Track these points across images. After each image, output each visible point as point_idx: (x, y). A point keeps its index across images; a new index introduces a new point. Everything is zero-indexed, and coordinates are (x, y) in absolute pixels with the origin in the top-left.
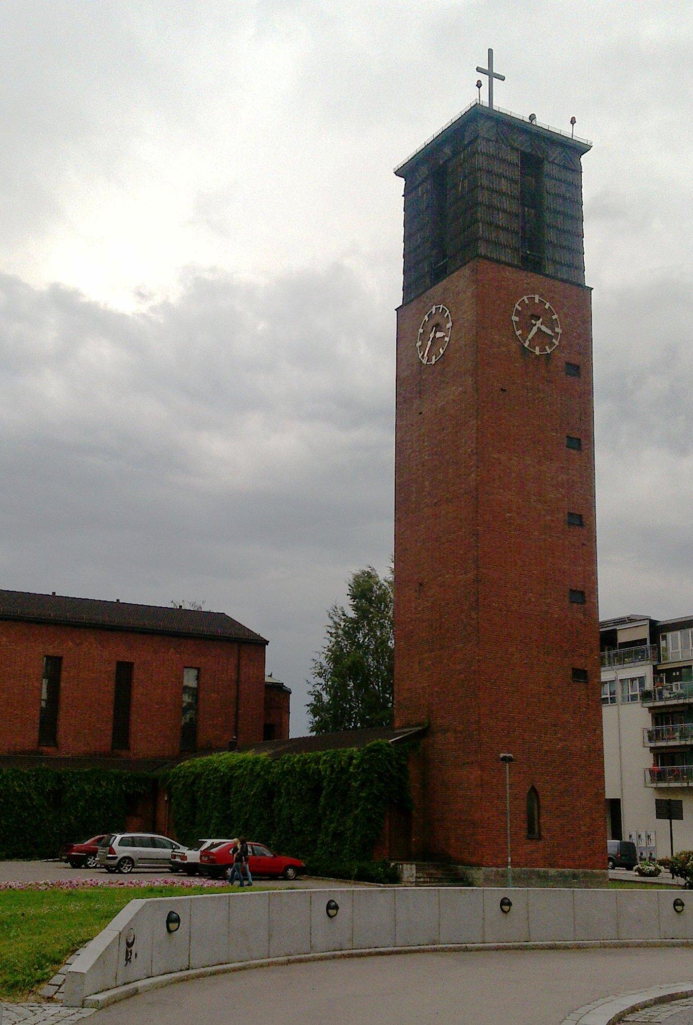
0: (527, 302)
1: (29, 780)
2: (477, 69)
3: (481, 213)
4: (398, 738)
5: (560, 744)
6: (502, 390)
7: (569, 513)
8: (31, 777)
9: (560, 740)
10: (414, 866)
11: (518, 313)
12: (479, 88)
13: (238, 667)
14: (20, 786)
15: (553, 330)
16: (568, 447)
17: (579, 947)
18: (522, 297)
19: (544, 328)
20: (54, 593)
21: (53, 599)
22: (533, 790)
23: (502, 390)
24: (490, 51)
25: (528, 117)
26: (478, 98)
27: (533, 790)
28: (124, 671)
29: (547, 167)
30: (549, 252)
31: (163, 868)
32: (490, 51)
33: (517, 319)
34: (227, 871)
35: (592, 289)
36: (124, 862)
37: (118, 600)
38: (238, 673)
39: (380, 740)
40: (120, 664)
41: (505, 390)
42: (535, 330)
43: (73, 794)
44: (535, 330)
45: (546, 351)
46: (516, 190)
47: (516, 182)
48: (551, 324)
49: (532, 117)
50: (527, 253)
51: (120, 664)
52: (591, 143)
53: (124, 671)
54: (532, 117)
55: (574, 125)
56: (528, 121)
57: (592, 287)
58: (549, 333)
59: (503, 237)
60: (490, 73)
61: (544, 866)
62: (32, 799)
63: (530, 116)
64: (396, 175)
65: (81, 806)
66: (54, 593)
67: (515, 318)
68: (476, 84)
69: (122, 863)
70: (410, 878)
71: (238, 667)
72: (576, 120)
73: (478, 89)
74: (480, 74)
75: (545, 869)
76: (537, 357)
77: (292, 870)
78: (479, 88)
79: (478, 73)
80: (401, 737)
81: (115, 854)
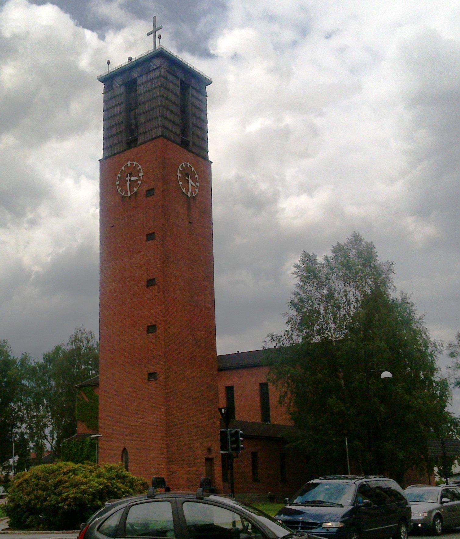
19: (132, 178)
44: (128, 183)
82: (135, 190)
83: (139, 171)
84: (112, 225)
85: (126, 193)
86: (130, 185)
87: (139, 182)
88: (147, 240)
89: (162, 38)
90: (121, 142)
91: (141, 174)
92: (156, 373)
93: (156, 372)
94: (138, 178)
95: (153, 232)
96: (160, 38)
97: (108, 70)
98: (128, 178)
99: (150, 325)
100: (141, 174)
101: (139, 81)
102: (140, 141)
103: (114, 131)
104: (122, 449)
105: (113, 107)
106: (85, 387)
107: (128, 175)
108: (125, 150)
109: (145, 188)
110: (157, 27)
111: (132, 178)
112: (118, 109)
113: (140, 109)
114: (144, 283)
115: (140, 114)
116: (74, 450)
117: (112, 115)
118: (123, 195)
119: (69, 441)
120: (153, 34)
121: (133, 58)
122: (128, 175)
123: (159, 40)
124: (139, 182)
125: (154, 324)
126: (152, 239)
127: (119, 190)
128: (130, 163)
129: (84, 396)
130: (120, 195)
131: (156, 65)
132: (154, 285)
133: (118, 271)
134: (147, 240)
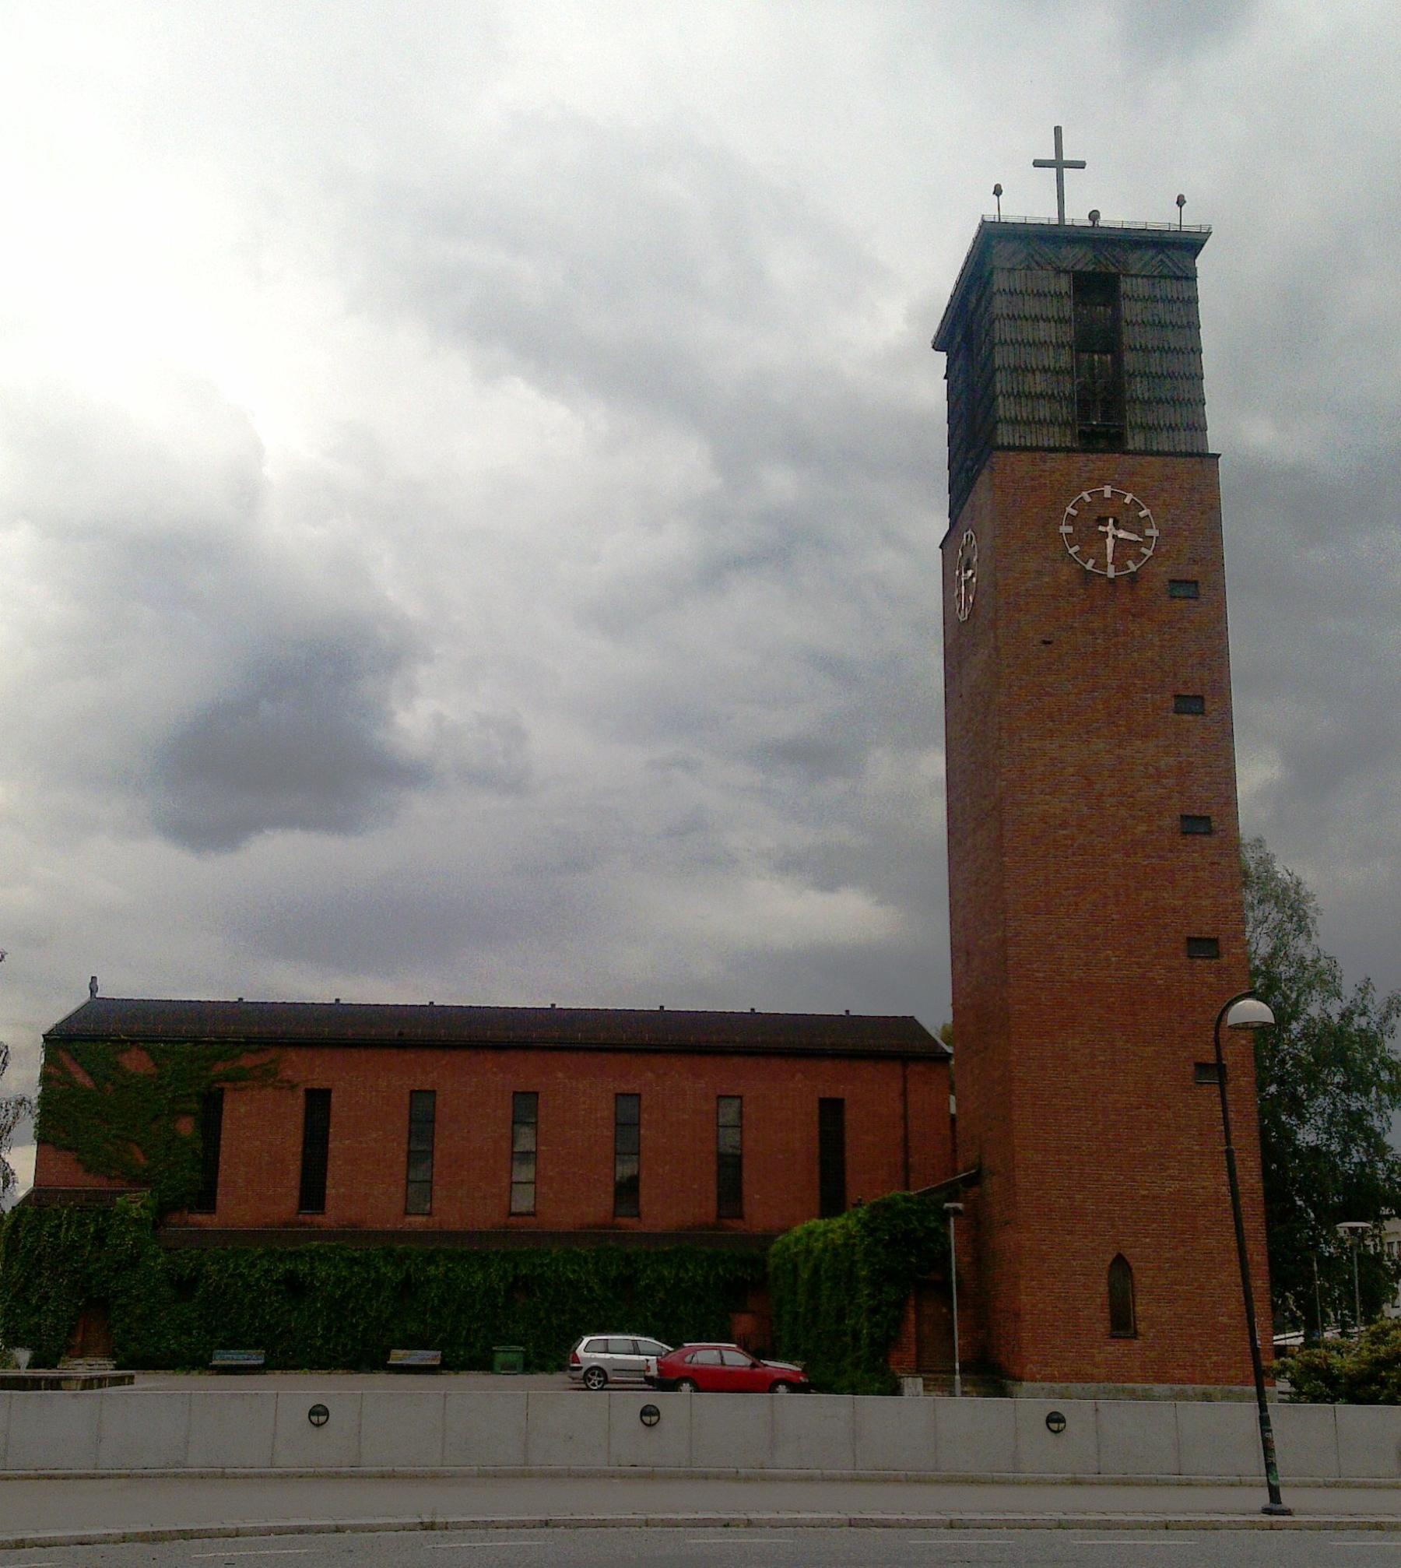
0: (1088, 499)
1: (586, 1263)
2: (1034, 163)
3: (1002, 382)
6: (1045, 642)
7: (1182, 816)
8: (590, 1259)
9: (1172, 1178)
10: (920, 1380)
11: (1071, 520)
12: (998, 196)
13: (904, 1094)
14: (574, 1271)
15: (1140, 533)
16: (1177, 712)
17: (435, 1476)
18: (1080, 494)
19: (1122, 534)
21: (662, 1015)
23: (1045, 642)
24: (1058, 130)
25: (1087, 218)
26: (997, 214)
28: (831, 1110)
29: (1126, 285)
30: (1135, 415)
31: (629, 1383)
32: (1058, 130)
34: (684, 1384)
35: (1219, 455)
36: (593, 1374)
37: (753, 1010)
38: (905, 1103)
40: (823, 1102)
41: (1049, 643)
42: (1110, 542)
43: (647, 1281)
44: (1110, 542)
46: (1068, 334)
47: (1067, 321)
48: (1139, 526)
49: (1094, 215)
50: (1094, 425)
51: (823, 1102)
52: (1210, 228)
53: (831, 1110)
54: (1094, 215)
55: (1183, 208)
56: (1090, 224)
57: (1219, 453)
58: (1132, 539)
59: (1044, 411)
60: (1059, 164)
61: (1146, 1380)
62: (591, 1290)
63: (1089, 216)
64: (936, 350)
65: (660, 1298)
67: (1066, 529)
68: (993, 190)
69: (590, 1376)
71: (904, 1094)
72: (1186, 199)
73: (996, 197)
75: (1147, 1386)
76: (1111, 581)
77: (688, 1385)
78: (998, 196)
79: (1037, 168)
81: (579, 1363)
98: (1110, 528)
102: (1136, 441)
104: (1110, 1258)
107: (1111, 521)
114: (1169, 821)
118: (1089, 566)
123: (1179, 208)
129: (74, 1068)
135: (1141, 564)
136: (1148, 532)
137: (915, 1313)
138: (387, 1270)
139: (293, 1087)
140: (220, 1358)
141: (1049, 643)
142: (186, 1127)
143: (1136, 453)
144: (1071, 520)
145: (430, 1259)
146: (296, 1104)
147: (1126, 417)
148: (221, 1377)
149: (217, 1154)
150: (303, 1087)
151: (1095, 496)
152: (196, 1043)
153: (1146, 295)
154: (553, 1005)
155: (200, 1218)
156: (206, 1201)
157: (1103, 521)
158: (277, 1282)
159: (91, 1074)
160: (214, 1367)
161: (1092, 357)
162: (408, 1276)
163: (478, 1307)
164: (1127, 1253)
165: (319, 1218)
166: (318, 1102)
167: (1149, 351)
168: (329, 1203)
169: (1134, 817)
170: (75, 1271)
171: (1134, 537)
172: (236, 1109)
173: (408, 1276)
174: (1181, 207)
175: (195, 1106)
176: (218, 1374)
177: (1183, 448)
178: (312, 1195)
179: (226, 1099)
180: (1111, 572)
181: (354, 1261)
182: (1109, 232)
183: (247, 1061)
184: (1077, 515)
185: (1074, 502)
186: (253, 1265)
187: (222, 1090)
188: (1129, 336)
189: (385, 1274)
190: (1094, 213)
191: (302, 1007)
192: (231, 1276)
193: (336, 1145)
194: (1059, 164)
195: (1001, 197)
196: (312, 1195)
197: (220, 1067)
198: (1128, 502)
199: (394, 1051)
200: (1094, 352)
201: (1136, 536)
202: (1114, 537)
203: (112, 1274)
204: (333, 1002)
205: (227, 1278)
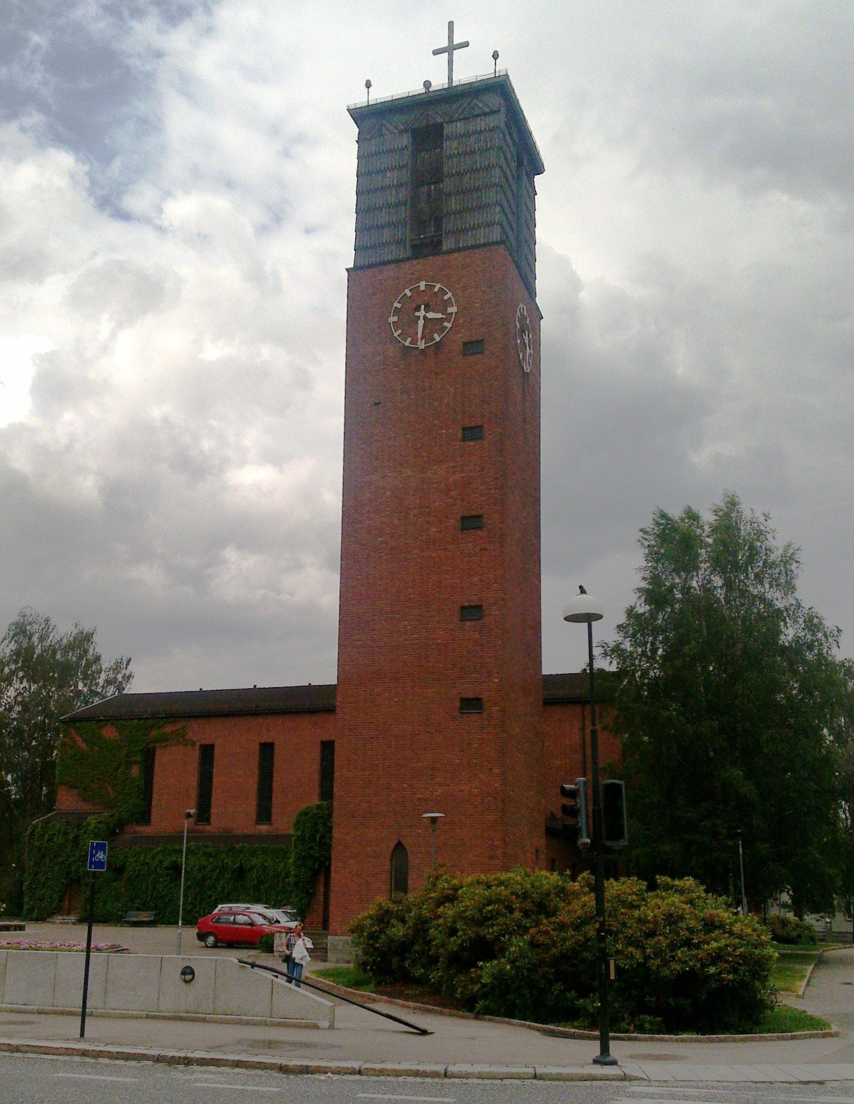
2: (433, 52)
4: (741, 862)
5: (439, 790)
9: (440, 785)
11: (397, 311)
19: (431, 315)
20: (255, 686)
22: (399, 845)
24: (451, 24)
27: (399, 845)
32: (451, 24)
33: (422, 288)
37: (255, 686)
39: (817, 855)
41: (379, 403)
42: (421, 322)
44: (421, 322)
45: (450, 298)
53: (267, 749)
54: (427, 84)
66: (255, 686)
67: (422, 285)
70: (279, 947)
74: (438, 55)
79: (447, 24)
80: (741, 848)
82: (437, 338)
83: (448, 303)
84: (377, 401)
85: (414, 341)
86: (424, 327)
87: (448, 325)
88: (464, 440)
89: (499, 58)
90: (401, 242)
91: (453, 309)
92: (480, 699)
93: (480, 697)
94: (444, 316)
95: (480, 424)
96: (496, 57)
97: (367, 100)
98: (422, 313)
99: (466, 604)
100: (453, 309)
101: (448, 130)
102: (447, 245)
103: (383, 217)
104: (392, 845)
105: (383, 171)
106: (82, 721)
107: (423, 307)
108: (408, 259)
109: (461, 337)
110: (457, 40)
111: (431, 315)
112: (391, 178)
113: (448, 185)
114: (453, 523)
115: (450, 195)
116: (60, 840)
117: (372, 187)
118: (407, 344)
119: (47, 822)
120: (447, 54)
121: (433, 84)
122: (423, 307)
123: (494, 61)
124: (448, 325)
125: (478, 603)
126: (478, 439)
127: (396, 334)
128: (410, 290)
129: (78, 738)
130: (398, 345)
131: (489, 107)
132: (480, 528)
133: (388, 494)
134: (464, 440)
135: (443, 335)
136: (450, 310)
137: (324, 888)
138: (228, 861)
139: (193, 744)
140: (133, 916)
141: (379, 403)
142: (135, 771)
143: (450, 252)
144: (397, 311)
145: (253, 854)
146: (195, 755)
147: (442, 228)
148: (133, 928)
149: (151, 788)
150: (198, 744)
151: (414, 290)
152: (140, 719)
153: (462, 133)
154: (255, 686)
155: (140, 829)
156: (145, 817)
157: (418, 309)
158: (167, 868)
159: (86, 741)
160: (127, 922)
161: (430, 187)
162: (241, 864)
163: (281, 885)
164: (407, 842)
165: (207, 828)
166: (207, 753)
167: (462, 174)
168: (213, 818)
169: (428, 523)
170: (62, 863)
171: (440, 316)
172: (163, 759)
173: (241, 864)
174: (496, 60)
175: (138, 758)
176: (131, 926)
177: (482, 241)
178: (204, 812)
179: (157, 753)
180: (422, 345)
181: (209, 855)
182: (463, 88)
183: (168, 729)
184: (401, 307)
185: (399, 298)
186: (154, 858)
187: (154, 747)
188: (451, 166)
189: (227, 863)
190: (426, 83)
191: (248, 690)
192: (142, 865)
193: (218, 780)
194: (450, 49)
195: (370, 89)
196: (204, 812)
197: (155, 733)
198: (424, 289)
199: (250, 719)
200: (430, 184)
201: (440, 314)
202: (425, 318)
203: (81, 864)
204: (253, 687)
205: (140, 866)
